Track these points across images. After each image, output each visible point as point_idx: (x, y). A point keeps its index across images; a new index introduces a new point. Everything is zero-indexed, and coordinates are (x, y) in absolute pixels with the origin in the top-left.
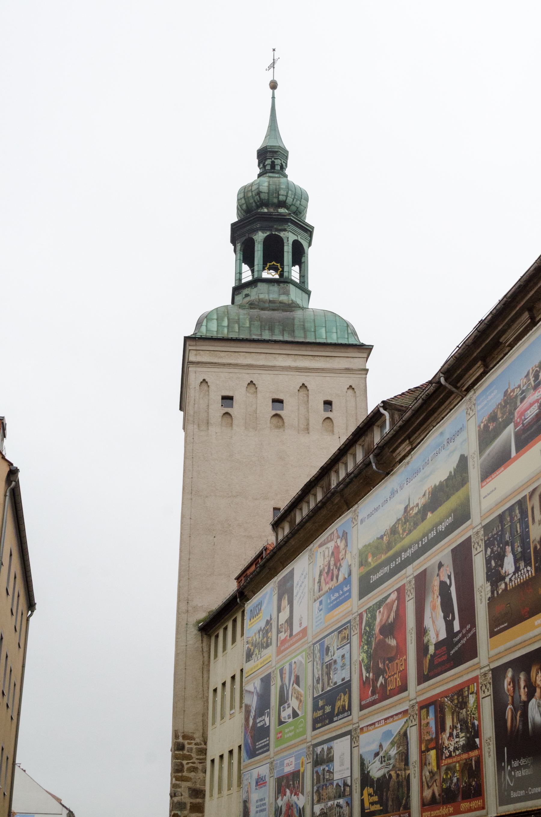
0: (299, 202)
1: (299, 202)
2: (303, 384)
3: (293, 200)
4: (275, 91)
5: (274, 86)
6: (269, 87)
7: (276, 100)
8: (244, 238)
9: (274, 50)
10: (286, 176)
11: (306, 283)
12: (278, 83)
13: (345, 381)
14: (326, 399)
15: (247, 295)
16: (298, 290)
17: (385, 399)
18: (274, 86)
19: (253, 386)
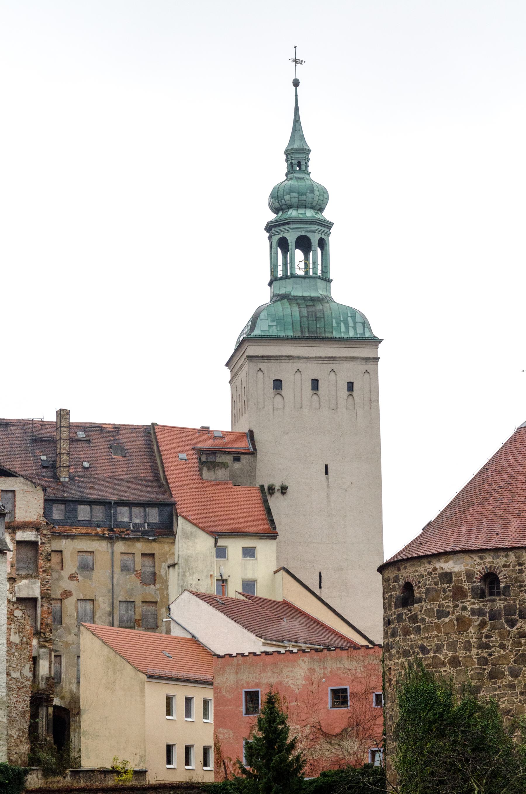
0: (283, 201)
1: (283, 201)
2: (333, 370)
3: (278, 202)
4: (298, 88)
5: (296, 83)
6: (292, 84)
7: (298, 97)
8: (300, 234)
9: (295, 47)
10: (309, 174)
11: (328, 273)
12: (300, 82)
13: (361, 367)
14: (349, 381)
15: (139, 783)
16: (323, 282)
17: (380, 362)
18: (296, 83)
19: (299, 372)
